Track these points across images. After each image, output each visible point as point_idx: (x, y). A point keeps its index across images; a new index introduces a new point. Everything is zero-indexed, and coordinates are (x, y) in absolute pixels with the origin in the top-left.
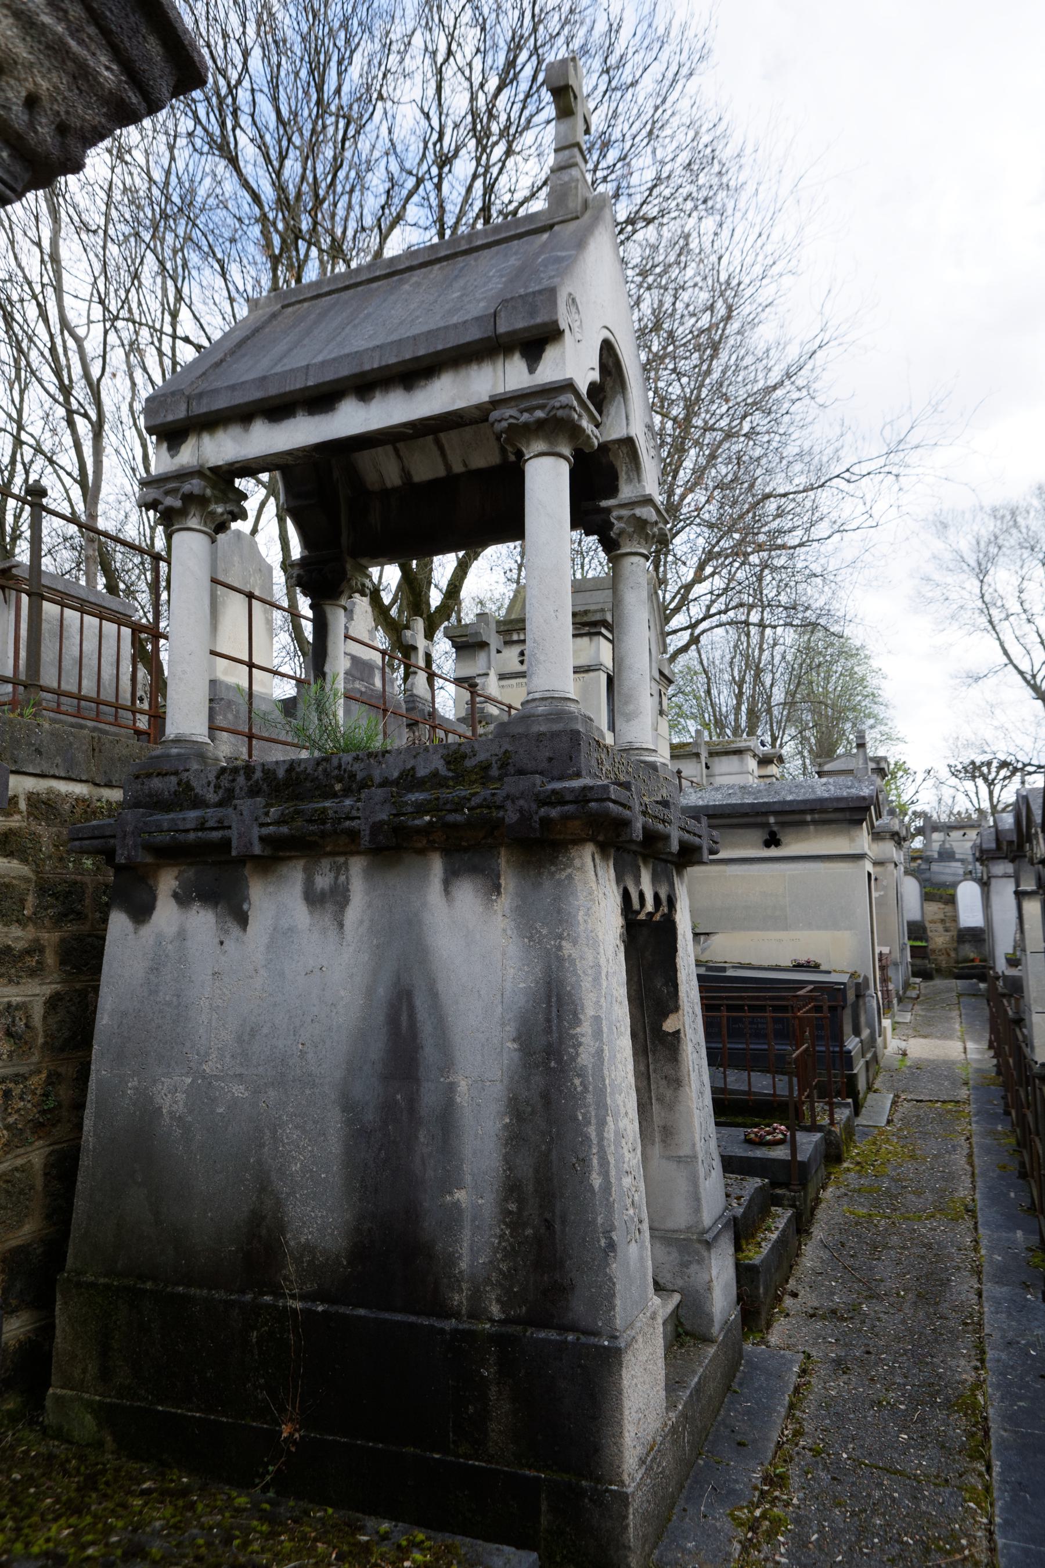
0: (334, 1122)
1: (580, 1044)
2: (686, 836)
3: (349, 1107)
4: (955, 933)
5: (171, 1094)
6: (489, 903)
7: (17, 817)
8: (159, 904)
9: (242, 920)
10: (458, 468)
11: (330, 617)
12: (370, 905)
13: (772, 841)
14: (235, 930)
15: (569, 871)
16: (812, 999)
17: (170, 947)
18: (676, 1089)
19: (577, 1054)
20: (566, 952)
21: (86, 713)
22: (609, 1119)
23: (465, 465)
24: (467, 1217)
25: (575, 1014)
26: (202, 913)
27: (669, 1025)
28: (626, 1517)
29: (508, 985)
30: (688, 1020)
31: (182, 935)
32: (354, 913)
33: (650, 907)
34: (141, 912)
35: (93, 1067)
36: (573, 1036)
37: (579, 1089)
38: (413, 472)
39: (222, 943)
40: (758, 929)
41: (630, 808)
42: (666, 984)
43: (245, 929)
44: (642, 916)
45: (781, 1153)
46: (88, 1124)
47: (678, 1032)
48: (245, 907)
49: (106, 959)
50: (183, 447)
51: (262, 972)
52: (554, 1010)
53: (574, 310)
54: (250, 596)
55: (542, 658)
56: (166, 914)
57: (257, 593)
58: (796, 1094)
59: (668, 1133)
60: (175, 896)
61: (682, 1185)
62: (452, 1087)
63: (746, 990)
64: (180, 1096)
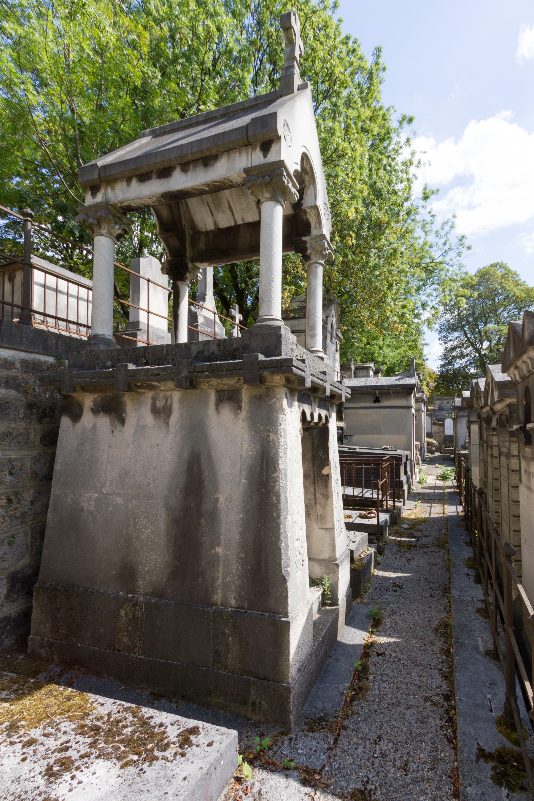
0: (163, 514)
1: (276, 481)
2: (334, 389)
3: (168, 508)
4: (443, 437)
5: (88, 500)
6: (236, 415)
7: (14, 371)
8: (84, 413)
9: (123, 421)
10: (240, 222)
11: (181, 289)
12: (181, 415)
13: (377, 400)
14: (119, 426)
15: (274, 400)
16: (390, 461)
17: (89, 433)
18: (326, 499)
19: (275, 486)
20: (271, 438)
21: (71, 330)
22: (289, 516)
23: (243, 220)
24: (222, 559)
25: (274, 467)
26: (104, 418)
27: (325, 472)
28: (289, 698)
29: (244, 453)
30: (333, 470)
31: (94, 428)
32: (174, 418)
33: (316, 420)
34: (76, 417)
35: (52, 489)
36: (274, 478)
37: (275, 502)
38: (219, 223)
39: (113, 432)
40: (370, 434)
41: (304, 371)
42: (324, 454)
43: (123, 425)
44: (312, 424)
45: (374, 521)
46: (49, 515)
47: (328, 475)
48: (124, 415)
49: (59, 439)
50: (98, 194)
51: (131, 446)
52: (265, 465)
53: (287, 129)
54: (149, 281)
55: (265, 299)
56: (88, 418)
57: (151, 279)
58: (380, 497)
59: (323, 518)
60: (92, 410)
61: (328, 540)
62: (217, 500)
63: (363, 457)
64: (93, 503)
